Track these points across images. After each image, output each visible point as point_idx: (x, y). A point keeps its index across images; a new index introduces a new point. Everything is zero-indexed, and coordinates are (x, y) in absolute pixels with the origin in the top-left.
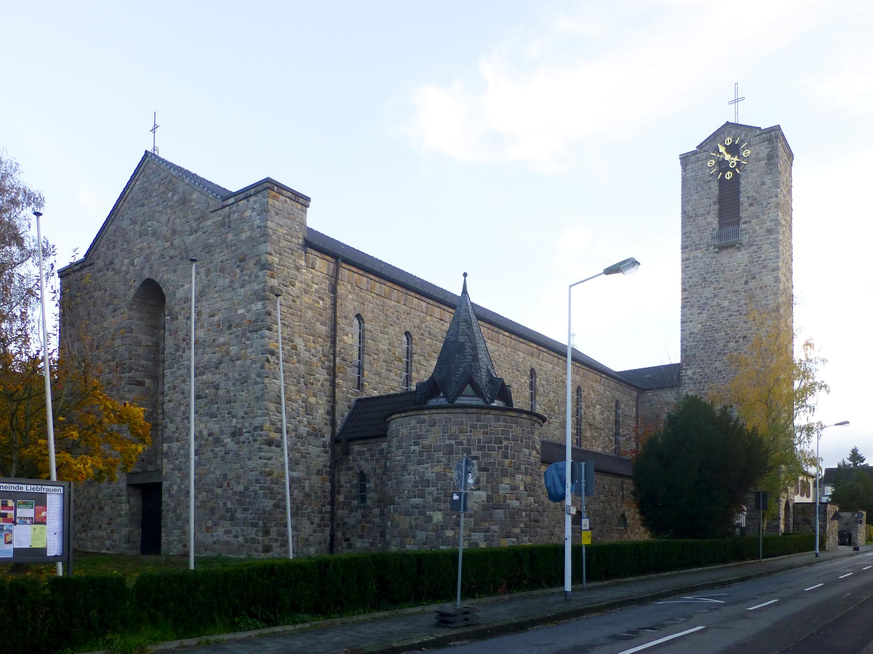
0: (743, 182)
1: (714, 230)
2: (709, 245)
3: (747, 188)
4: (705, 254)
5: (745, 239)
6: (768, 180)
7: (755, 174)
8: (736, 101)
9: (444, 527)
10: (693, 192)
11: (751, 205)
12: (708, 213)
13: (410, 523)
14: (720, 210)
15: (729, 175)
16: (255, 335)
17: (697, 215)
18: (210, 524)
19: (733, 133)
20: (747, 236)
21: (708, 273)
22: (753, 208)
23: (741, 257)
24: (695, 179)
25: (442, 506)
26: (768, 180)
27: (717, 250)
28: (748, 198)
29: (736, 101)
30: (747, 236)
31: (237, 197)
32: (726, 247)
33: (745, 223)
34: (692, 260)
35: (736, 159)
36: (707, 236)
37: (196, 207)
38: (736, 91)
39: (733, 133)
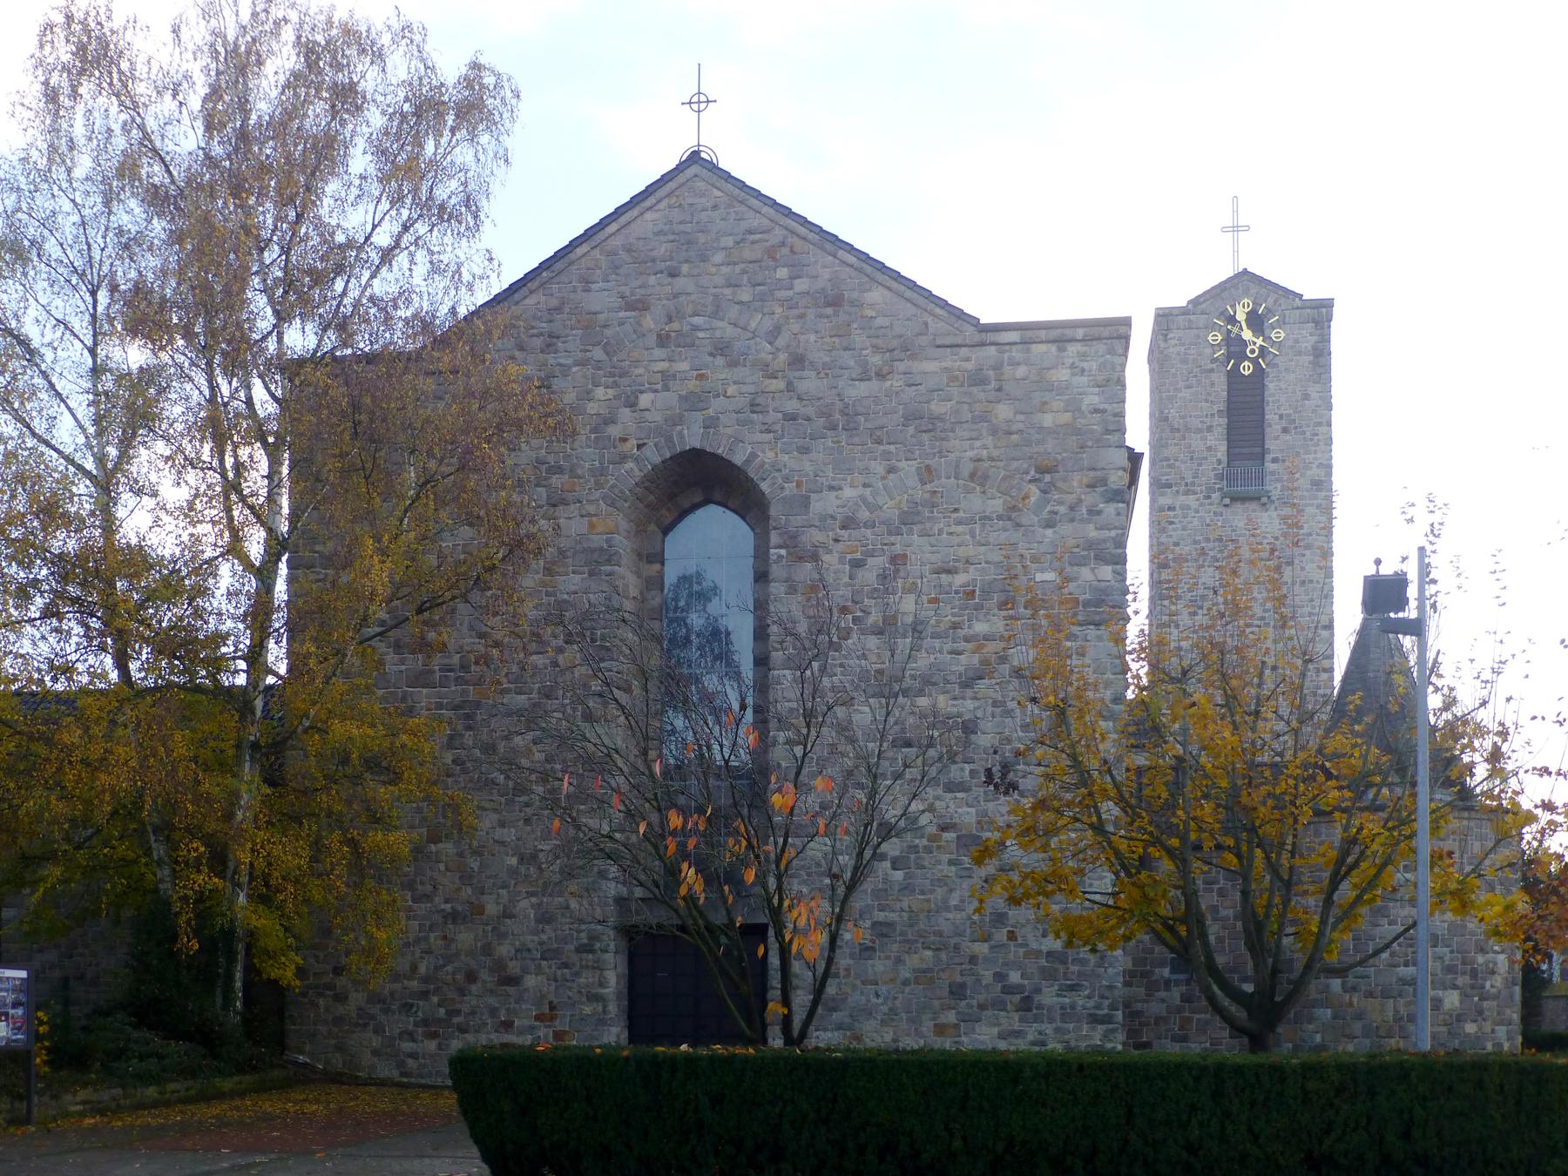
0: (1271, 386)
1: (1219, 461)
2: (1210, 490)
3: (1279, 397)
4: (1201, 505)
5: (1275, 489)
6: (1313, 390)
7: (1292, 377)
8: (1236, 229)
9: (1460, 1018)
10: (1181, 384)
11: (1285, 430)
12: (1210, 429)
13: (1396, 1012)
14: (1230, 428)
15: (1246, 369)
16: (1091, 632)
17: (1188, 429)
18: (950, 1017)
19: (1253, 291)
20: (1279, 486)
21: (1208, 540)
22: (1288, 437)
23: (1269, 522)
24: (1185, 361)
25: (1460, 981)
26: (1313, 390)
27: (1227, 501)
28: (1281, 417)
29: (1236, 229)
30: (1279, 486)
31: (1029, 333)
32: (1243, 499)
33: (1275, 460)
34: (1179, 512)
35: (1260, 342)
36: (1208, 472)
37: (880, 321)
38: (1235, 212)
39: (1253, 291)
